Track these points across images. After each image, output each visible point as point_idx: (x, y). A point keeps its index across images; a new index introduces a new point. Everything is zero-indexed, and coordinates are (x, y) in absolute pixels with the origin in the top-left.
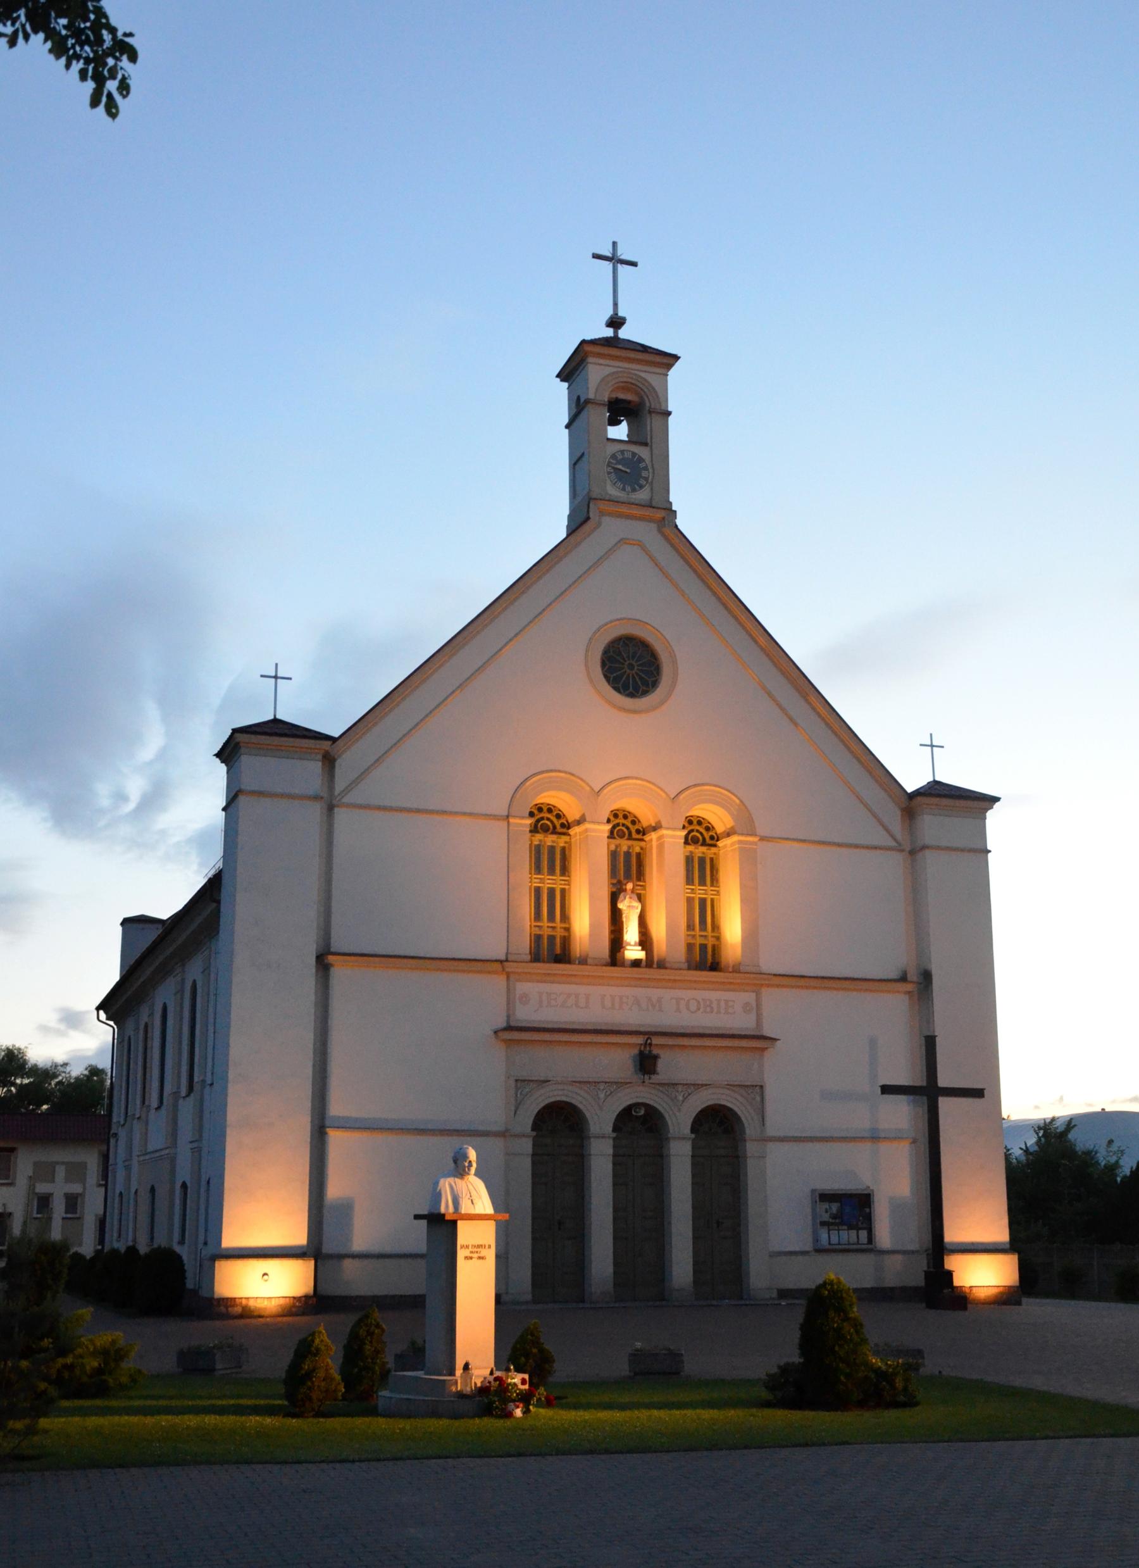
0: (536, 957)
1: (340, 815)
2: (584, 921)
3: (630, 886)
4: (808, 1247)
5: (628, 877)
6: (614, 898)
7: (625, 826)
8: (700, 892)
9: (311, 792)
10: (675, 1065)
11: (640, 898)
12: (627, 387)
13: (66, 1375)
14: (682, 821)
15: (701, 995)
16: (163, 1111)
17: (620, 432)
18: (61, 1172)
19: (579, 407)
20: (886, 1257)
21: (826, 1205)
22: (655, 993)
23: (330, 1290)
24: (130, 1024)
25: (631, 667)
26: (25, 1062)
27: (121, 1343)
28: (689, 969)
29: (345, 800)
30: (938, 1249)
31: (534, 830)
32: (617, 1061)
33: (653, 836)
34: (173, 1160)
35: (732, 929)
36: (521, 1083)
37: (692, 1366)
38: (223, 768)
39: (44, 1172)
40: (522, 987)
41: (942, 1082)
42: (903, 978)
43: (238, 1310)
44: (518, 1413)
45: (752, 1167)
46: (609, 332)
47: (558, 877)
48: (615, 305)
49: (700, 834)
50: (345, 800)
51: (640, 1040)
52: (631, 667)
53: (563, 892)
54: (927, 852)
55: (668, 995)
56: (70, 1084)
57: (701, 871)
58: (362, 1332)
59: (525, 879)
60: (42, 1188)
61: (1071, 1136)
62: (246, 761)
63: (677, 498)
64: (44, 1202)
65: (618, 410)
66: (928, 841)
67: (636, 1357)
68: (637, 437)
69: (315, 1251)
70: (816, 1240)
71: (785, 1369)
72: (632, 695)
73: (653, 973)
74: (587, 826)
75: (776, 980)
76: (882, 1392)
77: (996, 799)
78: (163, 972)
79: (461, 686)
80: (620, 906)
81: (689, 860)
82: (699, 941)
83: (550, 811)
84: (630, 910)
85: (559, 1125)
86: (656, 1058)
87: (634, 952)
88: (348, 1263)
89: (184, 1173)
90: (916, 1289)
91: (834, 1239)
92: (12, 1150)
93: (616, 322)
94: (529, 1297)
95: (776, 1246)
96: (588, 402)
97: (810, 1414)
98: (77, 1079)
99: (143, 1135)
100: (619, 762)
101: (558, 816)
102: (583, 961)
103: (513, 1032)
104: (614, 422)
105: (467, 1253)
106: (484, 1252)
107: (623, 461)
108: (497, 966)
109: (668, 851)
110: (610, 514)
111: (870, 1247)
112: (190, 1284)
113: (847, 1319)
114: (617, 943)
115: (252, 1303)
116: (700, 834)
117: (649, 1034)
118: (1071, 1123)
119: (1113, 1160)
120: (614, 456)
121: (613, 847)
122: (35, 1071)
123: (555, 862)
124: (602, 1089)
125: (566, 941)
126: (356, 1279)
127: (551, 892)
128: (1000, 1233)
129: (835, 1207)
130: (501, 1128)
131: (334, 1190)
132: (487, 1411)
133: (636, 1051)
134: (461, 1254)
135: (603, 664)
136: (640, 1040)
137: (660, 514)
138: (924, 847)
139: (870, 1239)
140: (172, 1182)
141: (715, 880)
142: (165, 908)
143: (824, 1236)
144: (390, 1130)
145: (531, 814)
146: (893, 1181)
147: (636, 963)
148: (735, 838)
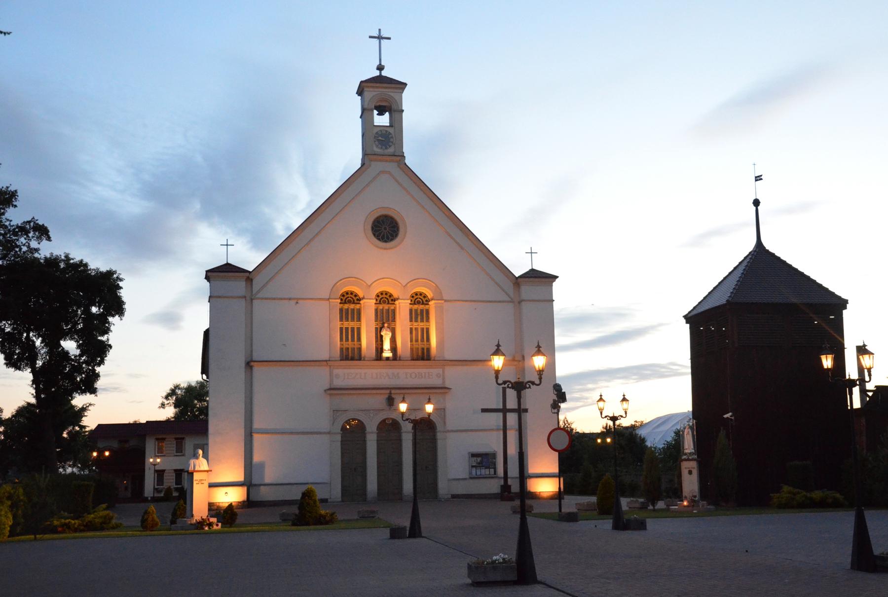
1: (255, 302)
2: (366, 341)
3: (386, 325)
5: (388, 320)
7: (385, 298)
14: (409, 297)
15: (417, 371)
22: (396, 371)
23: (255, 498)
25: (385, 229)
28: (413, 359)
29: (260, 295)
30: (523, 476)
32: (378, 401)
38: (208, 284)
40: (336, 371)
41: (501, 407)
44: (207, 528)
49: (419, 299)
51: (388, 391)
55: (401, 372)
69: (248, 483)
70: (470, 473)
72: (386, 242)
77: (557, 277)
84: (387, 336)
87: (387, 354)
88: (262, 487)
91: (479, 473)
92: (183, 438)
93: (380, 68)
95: (452, 476)
100: (380, 271)
101: (356, 296)
103: (333, 390)
104: (381, 113)
107: (382, 135)
109: (403, 307)
110: (376, 160)
114: (380, 350)
116: (419, 299)
123: (357, 316)
126: (265, 494)
127: (353, 329)
128: (555, 469)
129: (479, 459)
130: (328, 430)
131: (257, 458)
133: (387, 396)
134: (195, 483)
136: (388, 391)
137: (399, 158)
138: (523, 300)
139: (495, 473)
147: (388, 359)
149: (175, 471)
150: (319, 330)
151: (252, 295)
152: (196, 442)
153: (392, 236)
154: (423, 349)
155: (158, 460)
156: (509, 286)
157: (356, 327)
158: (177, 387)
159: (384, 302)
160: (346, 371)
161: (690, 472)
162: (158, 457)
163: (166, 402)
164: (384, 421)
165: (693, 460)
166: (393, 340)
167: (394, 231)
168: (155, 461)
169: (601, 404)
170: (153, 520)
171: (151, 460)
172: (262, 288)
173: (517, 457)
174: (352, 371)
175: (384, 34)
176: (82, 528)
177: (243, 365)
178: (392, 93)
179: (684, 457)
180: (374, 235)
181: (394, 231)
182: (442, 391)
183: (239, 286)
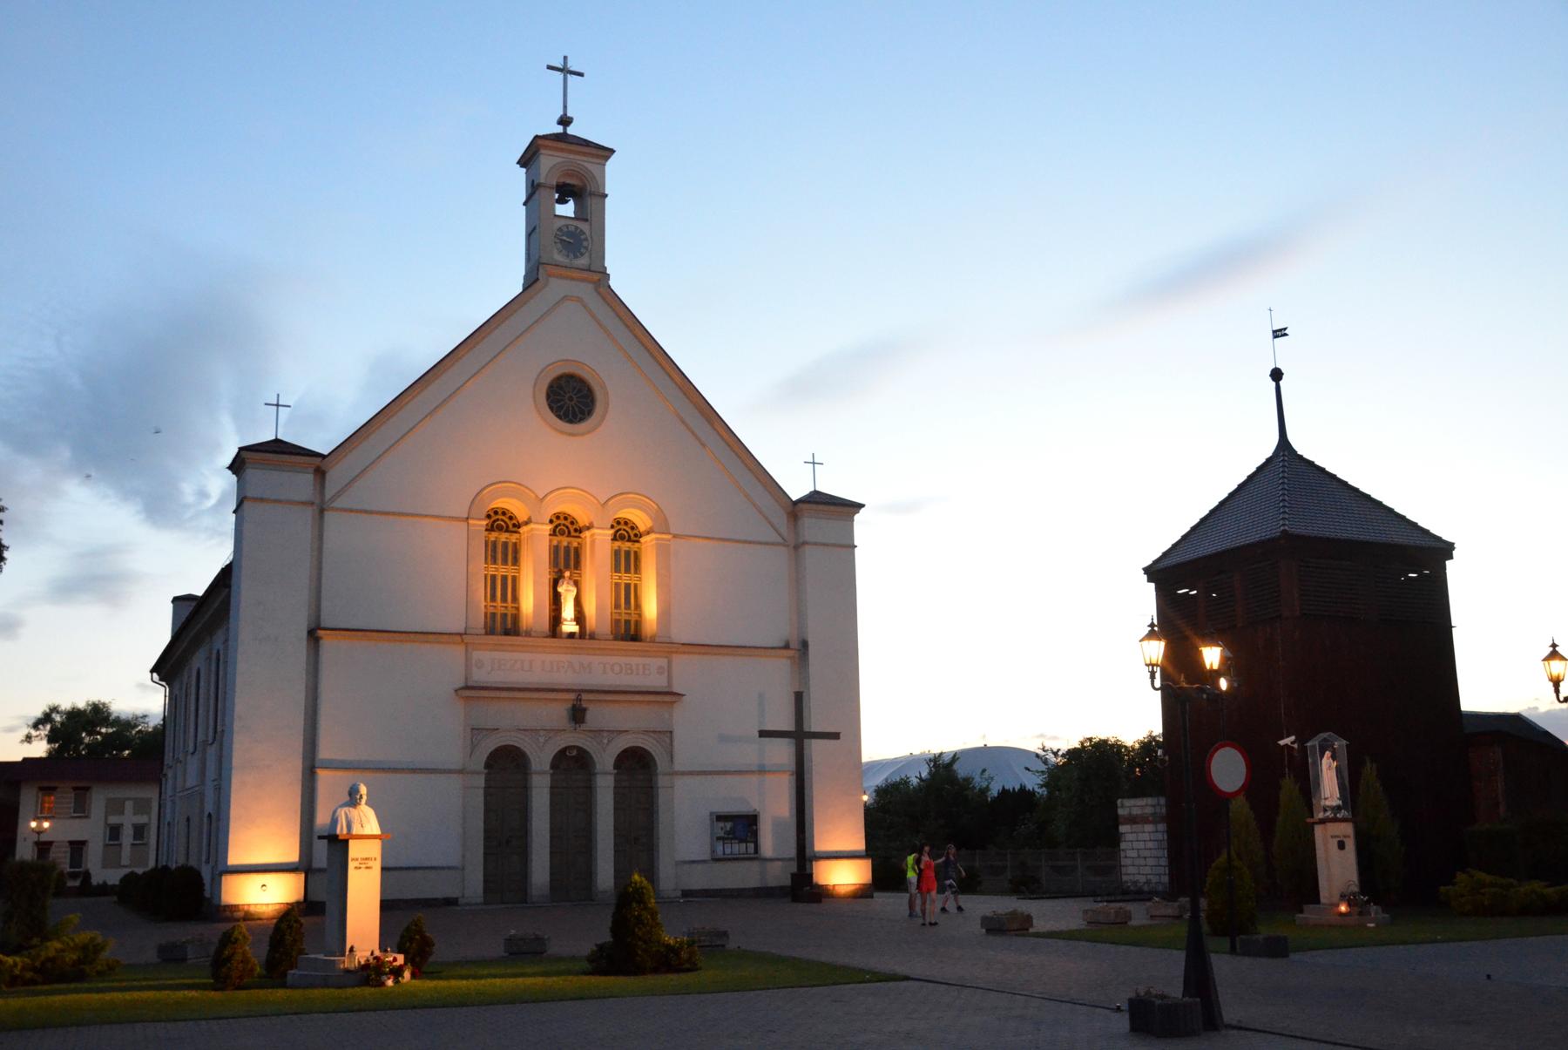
0: (490, 631)
1: (327, 515)
2: (530, 601)
3: (567, 574)
4: (707, 856)
5: (567, 567)
6: (555, 583)
7: (565, 526)
8: (625, 578)
9: (304, 498)
10: (598, 715)
11: (576, 584)
12: (569, 174)
13: (49, 965)
15: (623, 660)
16: (197, 756)
17: (567, 209)
18: (129, 805)
19: (533, 189)
20: (769, 864)
21: (721, 824)
22: (586, 659)
24: (177, 685)
25: (571, 399)
26: (109, 714)
27: (100, 939)
28: (615, 639)
29: (334, 505)
30: (805, 857)
31: (490, 529)
32: (556, 713)
33: (587, 534)
34: (202, 795)
35: (650, 608)
36: (476, 731)
37: (553, 949)
38: (234, 478)
39: (116, 807)
40: (476, 655)
42: (787, 647)
43: (241, 914)
44: (390, 983)
45: (662, 797)
46: (560, 129)
47: (510, 567)
48: (565, 107)
49: (625, 532)
50: (334, 505)
51: (572, 696)
52: (571, 399)
53: (514, 579)
54: (807, 548)
55: (596, 661)
56: (148, 733)
57: (627, 561)
58: (284, 926)
59: (480, 568)
60: (113, 820)
61: (955, 767)
62: (250, 473)
63: (611, 264)
64: (115, 832)
65: (565, 192)
66: (808, 538)
67: (510, 941)
68: (581, 215)
70: (713, 852)
71: (601, 947)
72: (571, 422)
73: (586, 643)
74: (532, 526)
75: (682, 649)
76: (669, 961)
78: (196, 643)
79: (430, 414)
80: (560, 589)
81: (617, 553)
82: (624, 617)
83: (504, 513)
85: (506, 765)
86: (585, 710)
87: (569, 626)
89: (209, 807)
90: (782, 888)
91: (728, 851)
92: (87, 789)
93: (565, 121)
94: (481, 900)
96: (539, 185)
97: (612, 978)
98: (155, 728)
99: (184, 773)
100: (559, 475)
101: (511, 518)
102: (528, 634)
103: (471, 691)
104: (562, 201)
105: (356, 864)
106: (370, 863)
107: (570, 234)
108: (458, 638)
109: (599, 546)
111: (756, 856)
112: (207, 894)
113: (645, 908)
114: (556, 619)
115: (252, 909)
116: (625, 532)
117: (580, 692)
118: (955, 757)
119: (984, 785)
120: (560, 229)
121: (555, 543)
122: (117, 722)
123: (512, 555)
124: (541, 735)
125: (516, 618)
127: (504, 578)
128: (859, 844)
129: (729, 825)
132: (366, 982)
133: (569, 705)
134: (351, 865)
135: (548, 397)
137: (596, 277)
138: (805, 543)
139: (756, 850)
140: (202, 811)
141: (637, 569)
142: (198, 586)
143: (719, 848)
144: (383, 770)
145: (489, 516)
146: (775, 807)
147: (571, 635)
148: (653, 536)
149: (71, 843)
150: (448, 575)
151: (322, 501)
152: (111, 795)
153: (575, 416)
154: (627, 622)
155: (46, 825)
156: (781, 520)
157: (499, 575)
158: (54, 709)
159: (562, 533)
160: (497, 655)
161: (1341, 846)
162: (46, 819)
163: (34, 733)
164: (563, 752)
165: (1344, 820)
166: (578, 602)
167: (575, 416)
168: (40, 825)
169: (1557, 667)
170: (245, 961)
171: (33, 824)
172: (338, 494)
173: (794, 820)
174: (507, 655)
175: (572, 66)
176: (29, 975)
177: (304, 634)
178: (589, 164)
179: (1321, 815)
180: (551, 408)
181: (582, 412)
182: (667, 698)
183: (301, 484)
